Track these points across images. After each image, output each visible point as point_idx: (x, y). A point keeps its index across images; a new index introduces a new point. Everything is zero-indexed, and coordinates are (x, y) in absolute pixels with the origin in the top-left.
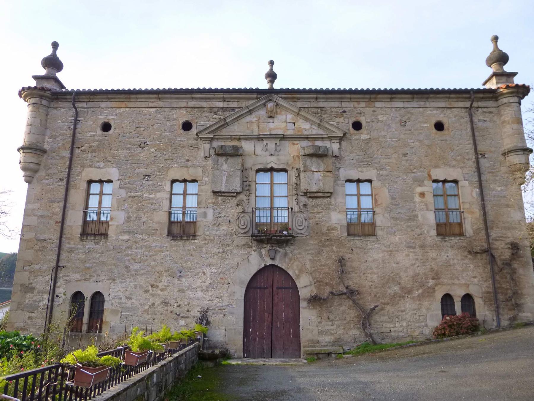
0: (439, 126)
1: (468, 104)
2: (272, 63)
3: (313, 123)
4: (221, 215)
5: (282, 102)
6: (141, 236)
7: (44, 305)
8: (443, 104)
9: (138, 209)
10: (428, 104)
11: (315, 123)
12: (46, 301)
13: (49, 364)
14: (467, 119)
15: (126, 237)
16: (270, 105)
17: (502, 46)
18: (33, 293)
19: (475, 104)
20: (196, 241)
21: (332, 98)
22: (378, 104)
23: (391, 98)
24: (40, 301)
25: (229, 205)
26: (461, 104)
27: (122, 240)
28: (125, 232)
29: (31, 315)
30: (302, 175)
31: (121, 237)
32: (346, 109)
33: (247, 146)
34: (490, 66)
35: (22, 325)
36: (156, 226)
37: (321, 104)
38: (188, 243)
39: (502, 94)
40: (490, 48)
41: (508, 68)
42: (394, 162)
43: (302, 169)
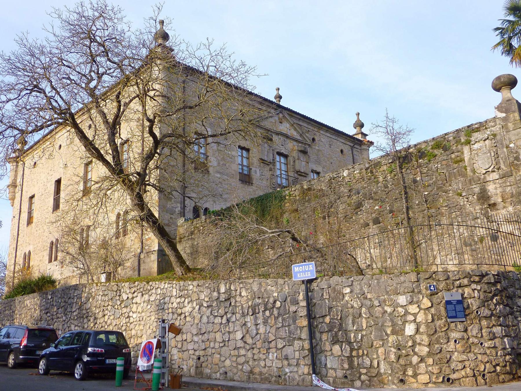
0: (342, 151)
1: (352, 145)
2: (278, 89)
3: (298, 132)
4: (263, 174)
5: (287, 116)
6: (226, 177)
7: (179, 211)
8: (343, 141)
9: (223, 159)
10: (339, 139)
11: (299, 132)
12: (179, 209)
13: (226, 379)
14: (351, 152)
15: (218, 175)
16: (281, 115)
17: (362, 119)
18: (171, 201)
19: (355, 146)
20: (253, 187)
21: (306, 122)
22: (321, 132)
23: (327, 131)
24: (176, 208)
25: (266, 169)
26: (349, 143)
27: (217, 177)
28: (218, 172)
29: (172, 216)
30: (297, 162)
31: (216, 175)
32: (310, 130)
33: (275, 138)
34: (355, 128)
35: (167, 222)
36: (233, 172)
37: (301, 123)
38: (249, 187)
39: (365, 144)
40: (356, 119)
41: (364, 130)
42: (490, 215)
43: (297, 158)
